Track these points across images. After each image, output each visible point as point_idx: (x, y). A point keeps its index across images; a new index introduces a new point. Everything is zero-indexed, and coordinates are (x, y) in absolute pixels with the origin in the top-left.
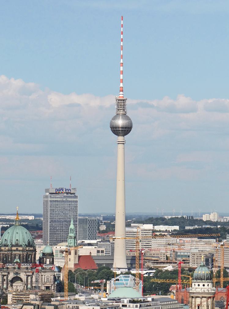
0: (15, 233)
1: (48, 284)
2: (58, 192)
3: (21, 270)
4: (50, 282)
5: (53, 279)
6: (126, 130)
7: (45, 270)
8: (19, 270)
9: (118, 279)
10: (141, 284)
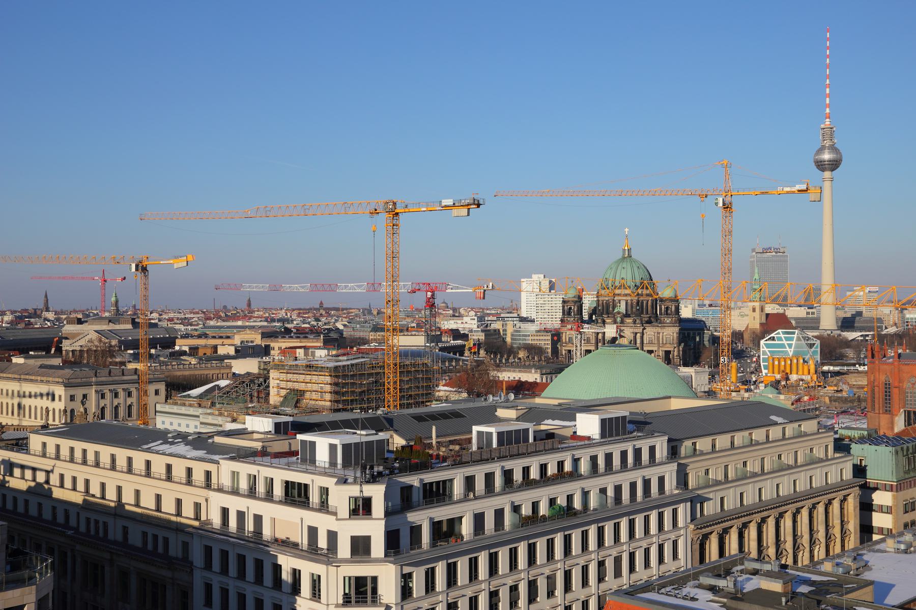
0: (620, 268)
1: (668, 347)
2: (765, 251)
3: (625, 325)
4: (671, 343)
6: (834, 165)
7: (662, 325)
8: (621, 325)
9: (774, 337)
10: (817, 345)
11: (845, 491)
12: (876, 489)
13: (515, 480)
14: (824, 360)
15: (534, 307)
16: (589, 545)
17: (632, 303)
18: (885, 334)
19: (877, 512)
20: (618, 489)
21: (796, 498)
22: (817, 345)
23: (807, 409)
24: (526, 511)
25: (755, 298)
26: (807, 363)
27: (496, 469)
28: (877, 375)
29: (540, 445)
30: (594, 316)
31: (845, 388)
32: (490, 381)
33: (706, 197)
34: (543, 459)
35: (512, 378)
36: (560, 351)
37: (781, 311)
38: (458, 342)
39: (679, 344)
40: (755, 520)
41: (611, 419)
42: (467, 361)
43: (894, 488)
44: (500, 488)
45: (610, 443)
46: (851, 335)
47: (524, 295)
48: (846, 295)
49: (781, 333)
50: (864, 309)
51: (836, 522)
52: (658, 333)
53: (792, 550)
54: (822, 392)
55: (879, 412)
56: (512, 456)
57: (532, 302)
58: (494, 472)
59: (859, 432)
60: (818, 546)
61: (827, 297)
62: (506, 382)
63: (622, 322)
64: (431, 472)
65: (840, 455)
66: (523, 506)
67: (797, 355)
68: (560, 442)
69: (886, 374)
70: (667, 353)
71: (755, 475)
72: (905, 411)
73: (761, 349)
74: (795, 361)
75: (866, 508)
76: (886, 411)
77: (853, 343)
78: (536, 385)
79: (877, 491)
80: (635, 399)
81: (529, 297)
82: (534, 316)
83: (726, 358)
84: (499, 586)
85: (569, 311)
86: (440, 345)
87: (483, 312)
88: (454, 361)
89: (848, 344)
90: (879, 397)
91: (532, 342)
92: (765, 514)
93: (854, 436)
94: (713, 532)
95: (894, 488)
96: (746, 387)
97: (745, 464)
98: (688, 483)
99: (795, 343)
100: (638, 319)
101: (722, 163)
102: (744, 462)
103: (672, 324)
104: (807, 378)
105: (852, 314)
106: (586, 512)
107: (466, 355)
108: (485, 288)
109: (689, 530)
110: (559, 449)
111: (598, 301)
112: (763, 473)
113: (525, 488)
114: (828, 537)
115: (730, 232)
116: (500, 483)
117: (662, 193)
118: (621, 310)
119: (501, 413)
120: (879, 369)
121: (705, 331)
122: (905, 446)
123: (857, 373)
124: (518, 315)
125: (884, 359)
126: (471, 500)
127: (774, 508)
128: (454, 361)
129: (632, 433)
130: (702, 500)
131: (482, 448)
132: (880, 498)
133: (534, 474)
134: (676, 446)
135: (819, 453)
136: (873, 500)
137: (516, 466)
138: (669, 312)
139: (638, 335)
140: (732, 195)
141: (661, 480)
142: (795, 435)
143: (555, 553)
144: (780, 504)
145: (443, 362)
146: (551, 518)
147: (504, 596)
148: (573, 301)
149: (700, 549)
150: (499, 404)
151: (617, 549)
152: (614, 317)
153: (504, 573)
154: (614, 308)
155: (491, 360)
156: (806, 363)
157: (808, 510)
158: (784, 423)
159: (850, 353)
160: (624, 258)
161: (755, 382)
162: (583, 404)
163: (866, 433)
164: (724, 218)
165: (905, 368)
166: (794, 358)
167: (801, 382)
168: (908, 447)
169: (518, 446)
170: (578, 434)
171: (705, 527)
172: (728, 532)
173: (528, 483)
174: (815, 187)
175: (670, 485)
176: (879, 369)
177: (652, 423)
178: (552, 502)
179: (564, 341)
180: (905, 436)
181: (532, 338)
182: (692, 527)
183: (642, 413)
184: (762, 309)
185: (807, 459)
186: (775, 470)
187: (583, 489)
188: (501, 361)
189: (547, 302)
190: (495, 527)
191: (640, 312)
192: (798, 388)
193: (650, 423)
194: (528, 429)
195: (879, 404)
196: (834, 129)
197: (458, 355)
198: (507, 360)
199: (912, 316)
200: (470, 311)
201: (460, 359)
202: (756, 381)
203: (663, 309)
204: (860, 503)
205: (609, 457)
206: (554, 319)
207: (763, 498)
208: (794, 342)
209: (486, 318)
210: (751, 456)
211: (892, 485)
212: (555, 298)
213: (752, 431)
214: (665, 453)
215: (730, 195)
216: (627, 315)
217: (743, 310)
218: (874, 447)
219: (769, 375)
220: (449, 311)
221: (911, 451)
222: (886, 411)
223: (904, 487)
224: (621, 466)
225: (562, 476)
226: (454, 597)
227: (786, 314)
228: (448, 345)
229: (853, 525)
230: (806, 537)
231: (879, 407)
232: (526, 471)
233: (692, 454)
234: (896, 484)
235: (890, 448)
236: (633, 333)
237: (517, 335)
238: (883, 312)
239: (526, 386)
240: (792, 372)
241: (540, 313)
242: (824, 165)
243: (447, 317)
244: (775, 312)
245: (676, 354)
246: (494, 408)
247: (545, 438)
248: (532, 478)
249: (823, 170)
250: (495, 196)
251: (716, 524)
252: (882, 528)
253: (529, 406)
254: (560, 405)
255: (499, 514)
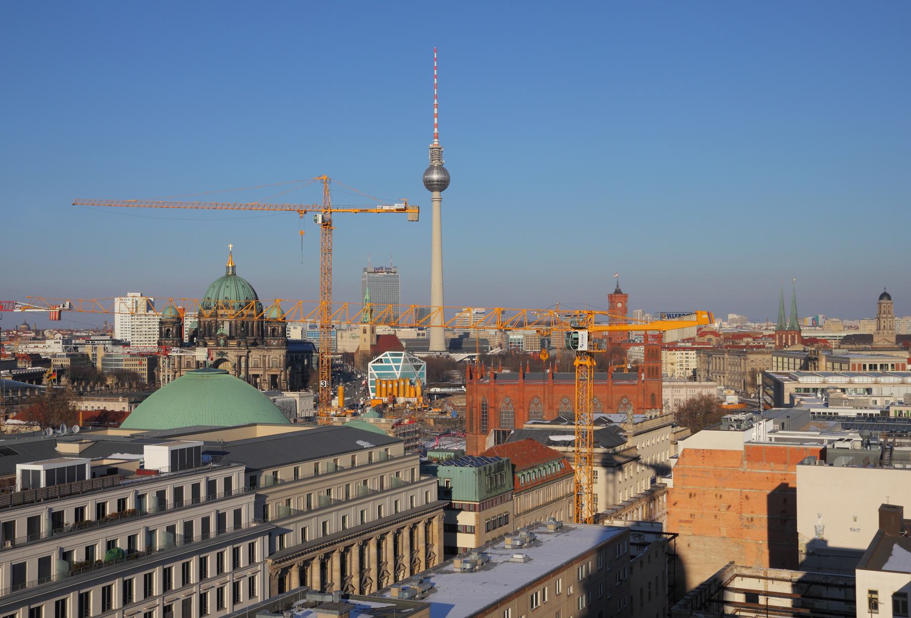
0: (223, 286)
1: (274, 371)
3: (229, 348)
4: (278, 366)
5: (284, 362)
6: (442, 185)
8: (224, 348)
9: (381, 359)
10: (424, 367)
11: (430, 514)
12: (460, 510)
13: (65, 524)
14: (432, 381)
15: (129, 329)
16: (255, 557)
17: (236, 324)
18: (490, 355)
19: (461, 532)
20: (188, 526)
21: (381, 524)
22: (424, 367)
23: (407, 432)
24: (78, 557)
25: (366, 318)
26: (414, 385)
27: (43, 513)
28: (475, 397)
29: (98, 482)
30: (195, 339)
31: (449, 408)
32: (68, 412)
33: (305, 213)
34: (100, 498)
35: (96, 408)
36: (156, 377)
37: (392, 333)
38: (37, 368)
39: (286, 367)
40: (338, 550)
41: (182, 451)
42: (44, 389)
43: (477, 508)
44: (47, 533)
45: (180, 476)
46: (458, 357)
47: (117, 318)
48: (455, 316)
49: (388, 355)
50: (471, 331)
51: (420, 545)
52: (264, 356)
53: (377, 578)
54: (428, 414)
55: (477, 432)
56: (63, 497)
57: (128, 324)
58: (39, 516)
59: (447, 454)
60: (403, 572)
61: (437, 319)
62: (83, 412)
63: (226, 345)
64: (11, 510)
65: (426, 478)
66: (75, 552)
67: (404, 377)
68: (123, 478)
69: (483, 395)
70: (274, 377)
71: (339, 502)
72: (495, 431)
73: (369, 372)
74: (402, 383)
75: (451, 529)
76: (483, 431)
77: (461, 364)
78: (122, 415)
79: (462, 512)
80: (213, 428)
81: (124, 318)
82: (129, 339)
83: (325, 382)
84: (172, 601)
85: (168, 333)
86: (14, 372)
87: (71, 334)
88: (28, 390)
89: (454, 365)
90: (477, 418)
91: (126, 368)
92: (349, 542)
93: (442, 458)
94: (389, 532)
95: (477, 508)
96: (353, 411)
97: (329, 492)
98: (267, 515)
99: (402, 365)
100: (242, 341)
101: (321, 178)
102: (327, 490)
103: (279, 347)
104: (414, 400)
105: (459, 336)
106: (149, 554)
107: (45, 383)
108: (61, 307)
109: (267, 566)
110: (121, 485)
111: (200, 322)
112: (382, 490)
113: (77, 531)
114: (428, 556)
115: (330, 251)
116: (47, 528)
117: (260, 208)
118: (224, 332)
119: (61, 448)
120: (477, 390)
121: (314, 354)
122: (488, 466)
123: (462, 394)
124: (111, 337)
125: (481, 380)
126: (8, 549)
127: (358, 536)
128: (28, 390)
129: (205, 464)
130: (282, 533)
131: (27, 489)
132: (465, 519)
133: (89, 515)
134: (256, 476)
135: (405, 477)
136: (457, 522)
137: (68, 509)
138: (276, 333)
139: (243, 358)
140: (331, 212)
141: (237, 514)
142: (381, 460)
143: (153, 589)
144: (364, 531)
145: (15, 391)
146: (108, 563)
147: (177, 609)
148: (171, 322)
149: (279, 584)
150: (61, 438)
151: (220, 580)
152: (217, 339)
153: (245, 566)
154: (216, 331)
155: (73, 388)
156: (413, 386)
157: (393, 536)
158: (370, 448)
159: (456, 374)
160: (228, 276)
161: (362, 406)
162: (159, 434)
163: (453, 454)
164: (324, 235)
165: (500, 388)
166: (401, 380)
167: (408, 405)
168: (490, 467)
169: (71, 485)
170: (146, 468)
171: (284, 561)
172: (310, 564)
173: (81, 525)
174: (413, 206)
175: (248, 518)
176: (477, 390)
177: (229, 453)
178: (110, 545)
179: (250, 366)
180: (489, 456)
181: (126, 363)
182: (270, 561)
183: (220, 442)
184: (373, 331)
185: (393, 484)
186: (360, 496)
187: (147, 528)
188: (85, 389)
189: (144, 323)
190: (39, 578)
191: (245, 334)
192: (405, 411)
193: (226, 453)
194: (84, 466)
195: (477, 425)
196: (442, 149)
197: (34, 383)
198: (92, 388)
199: (515, 337)
200: (56, 333)
201: (35, 388)
202: (364, 404)
203: (269, 330)
204: (445, 525)
205: (178, 492)
206: (152, 342)
207: (328, 533)
208: (401, 364)
209: (73, 342)
210: (295, 493)
211: (475, 505)
212: (153, 319)
213: (336, 458)
214: (242, 485)
215: (329, 212)
216: (231, 337)
217: (354, 331)
218: (459, 468)
219: (376, 398)
220: (31, 333)
221: (493, 470)
222: (483, 431)
223: (483, 508)
224: (225, 494)
225: (122, 516)
226: (149, 607)
227: (397, 336)
228: (24, 372)
229: (437, 548)
230: (391, 563)
231: (477, 428)
232: (80, 512)
233: (272, 484)
234: (478, 503)
235: (474, 469)
236: (237, 356)
237: (108, 360)
238: (488, 333)
239: (111, 417)
240: (400, 395)
241: (136, 336)
242: (433, 185)
243: (26, 340)
244: (386, 333)
245: (283, 378)
246: (54, 443)
247: (106, 474)
248: (87, 519)
249: (432, 190)
250: (73, 205)
251: (297, 556)
252: (466, 548)
253: (95, 439)
254: (132, 436)
255: (44, 563)
